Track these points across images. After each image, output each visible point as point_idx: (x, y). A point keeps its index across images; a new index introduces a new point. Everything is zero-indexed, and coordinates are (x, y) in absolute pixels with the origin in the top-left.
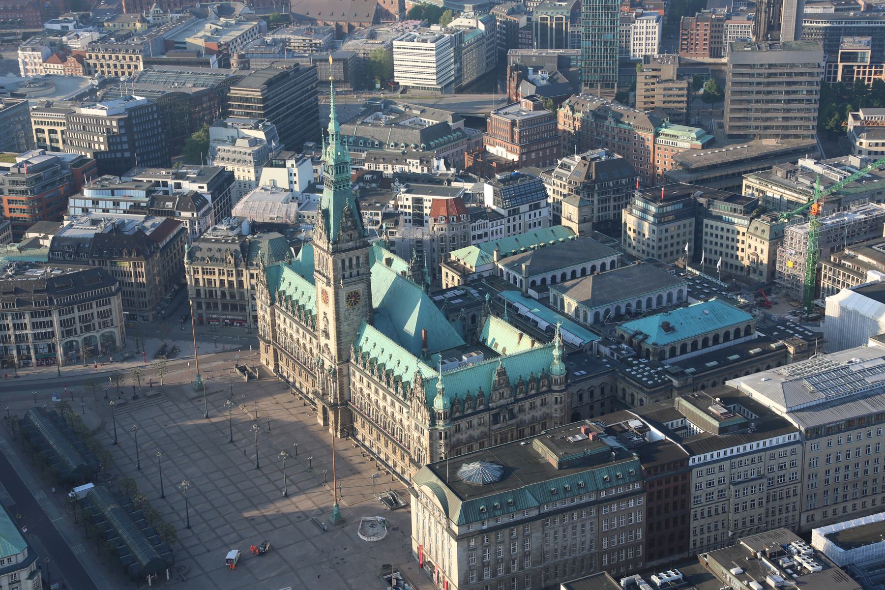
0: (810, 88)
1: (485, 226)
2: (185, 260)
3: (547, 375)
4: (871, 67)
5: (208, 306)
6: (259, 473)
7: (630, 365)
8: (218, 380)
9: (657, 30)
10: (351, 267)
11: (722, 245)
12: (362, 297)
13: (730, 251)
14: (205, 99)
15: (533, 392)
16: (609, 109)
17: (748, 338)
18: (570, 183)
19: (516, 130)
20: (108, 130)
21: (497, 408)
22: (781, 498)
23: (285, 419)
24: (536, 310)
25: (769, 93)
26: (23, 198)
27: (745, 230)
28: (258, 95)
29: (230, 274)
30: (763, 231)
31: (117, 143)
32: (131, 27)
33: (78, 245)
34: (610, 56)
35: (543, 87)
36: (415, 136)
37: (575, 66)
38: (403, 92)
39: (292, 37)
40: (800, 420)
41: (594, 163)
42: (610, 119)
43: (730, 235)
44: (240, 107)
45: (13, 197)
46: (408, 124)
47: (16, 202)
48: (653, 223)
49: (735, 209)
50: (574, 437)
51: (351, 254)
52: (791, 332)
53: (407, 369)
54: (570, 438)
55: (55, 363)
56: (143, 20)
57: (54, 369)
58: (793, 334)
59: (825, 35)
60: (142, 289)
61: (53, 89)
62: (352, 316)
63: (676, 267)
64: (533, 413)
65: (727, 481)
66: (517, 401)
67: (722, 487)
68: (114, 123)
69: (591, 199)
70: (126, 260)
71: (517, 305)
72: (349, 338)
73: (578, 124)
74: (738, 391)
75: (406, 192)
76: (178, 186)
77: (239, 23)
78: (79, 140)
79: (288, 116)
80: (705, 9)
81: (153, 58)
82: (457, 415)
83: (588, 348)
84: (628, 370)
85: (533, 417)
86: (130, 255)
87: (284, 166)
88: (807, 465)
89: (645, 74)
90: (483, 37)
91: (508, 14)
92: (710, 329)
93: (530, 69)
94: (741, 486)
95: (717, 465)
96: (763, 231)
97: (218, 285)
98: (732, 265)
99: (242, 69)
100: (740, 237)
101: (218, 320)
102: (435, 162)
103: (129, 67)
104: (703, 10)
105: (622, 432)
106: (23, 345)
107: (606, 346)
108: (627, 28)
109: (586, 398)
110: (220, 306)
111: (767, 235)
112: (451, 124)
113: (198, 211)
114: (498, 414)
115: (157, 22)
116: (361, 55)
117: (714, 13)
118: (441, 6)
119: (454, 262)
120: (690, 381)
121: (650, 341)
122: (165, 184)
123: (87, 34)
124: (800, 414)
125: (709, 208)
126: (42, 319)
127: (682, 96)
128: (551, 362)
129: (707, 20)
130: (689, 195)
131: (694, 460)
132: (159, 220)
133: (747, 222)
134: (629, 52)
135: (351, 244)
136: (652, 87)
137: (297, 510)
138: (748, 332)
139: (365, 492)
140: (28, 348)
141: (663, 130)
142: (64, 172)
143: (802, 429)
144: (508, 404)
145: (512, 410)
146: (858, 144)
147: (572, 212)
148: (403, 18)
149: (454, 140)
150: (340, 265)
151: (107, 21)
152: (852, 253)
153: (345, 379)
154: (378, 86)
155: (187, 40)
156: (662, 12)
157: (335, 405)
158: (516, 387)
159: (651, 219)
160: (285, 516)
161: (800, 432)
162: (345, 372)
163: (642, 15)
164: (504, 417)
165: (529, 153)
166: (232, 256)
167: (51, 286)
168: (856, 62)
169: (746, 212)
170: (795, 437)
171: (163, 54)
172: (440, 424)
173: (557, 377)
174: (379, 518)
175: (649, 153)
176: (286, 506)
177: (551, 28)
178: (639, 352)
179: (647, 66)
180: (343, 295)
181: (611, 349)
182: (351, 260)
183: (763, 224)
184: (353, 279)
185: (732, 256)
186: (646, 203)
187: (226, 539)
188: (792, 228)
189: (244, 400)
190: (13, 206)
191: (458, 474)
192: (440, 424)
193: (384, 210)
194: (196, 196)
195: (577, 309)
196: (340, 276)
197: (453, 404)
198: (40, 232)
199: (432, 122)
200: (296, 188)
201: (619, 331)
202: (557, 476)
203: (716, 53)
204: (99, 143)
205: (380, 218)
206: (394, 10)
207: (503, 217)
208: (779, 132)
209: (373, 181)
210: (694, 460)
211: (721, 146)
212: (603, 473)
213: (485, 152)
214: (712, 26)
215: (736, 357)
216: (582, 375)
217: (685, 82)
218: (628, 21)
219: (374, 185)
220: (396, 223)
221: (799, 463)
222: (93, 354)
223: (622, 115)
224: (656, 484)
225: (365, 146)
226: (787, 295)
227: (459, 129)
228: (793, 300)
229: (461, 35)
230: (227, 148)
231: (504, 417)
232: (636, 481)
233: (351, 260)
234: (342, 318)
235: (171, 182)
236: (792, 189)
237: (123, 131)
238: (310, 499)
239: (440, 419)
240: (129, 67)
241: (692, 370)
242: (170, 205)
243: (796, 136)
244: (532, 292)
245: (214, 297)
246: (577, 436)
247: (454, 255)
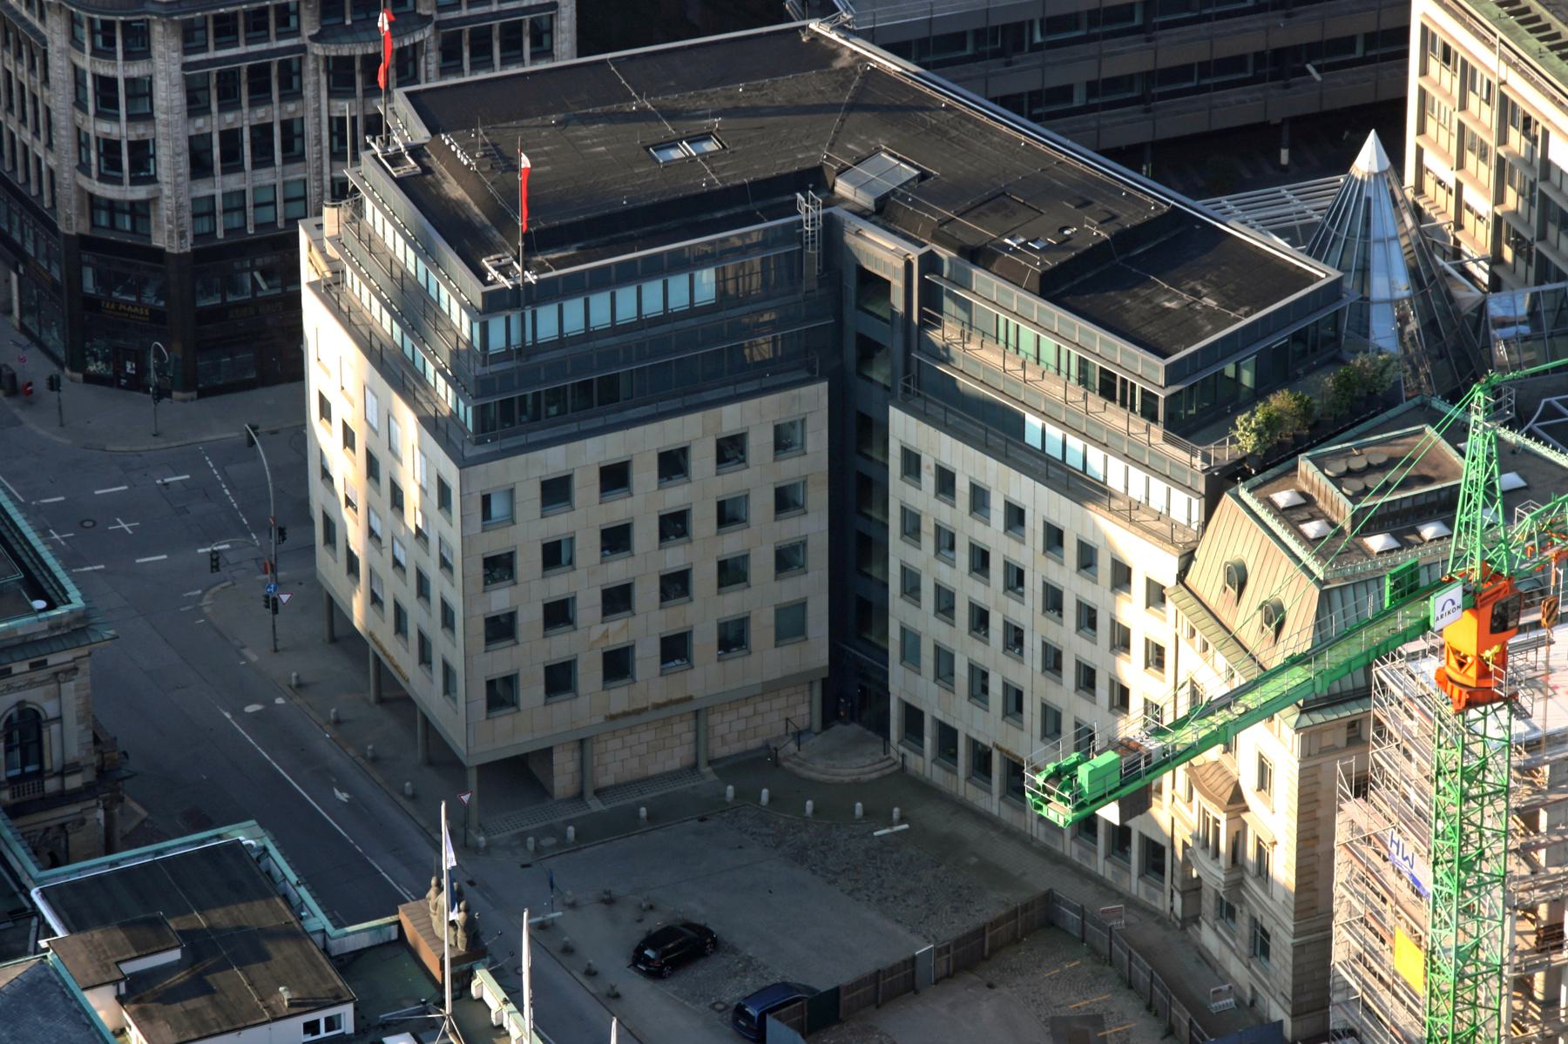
57: (122, 18)
100: (1131, 610)
125: (932, 320)
133: (1184, 507)
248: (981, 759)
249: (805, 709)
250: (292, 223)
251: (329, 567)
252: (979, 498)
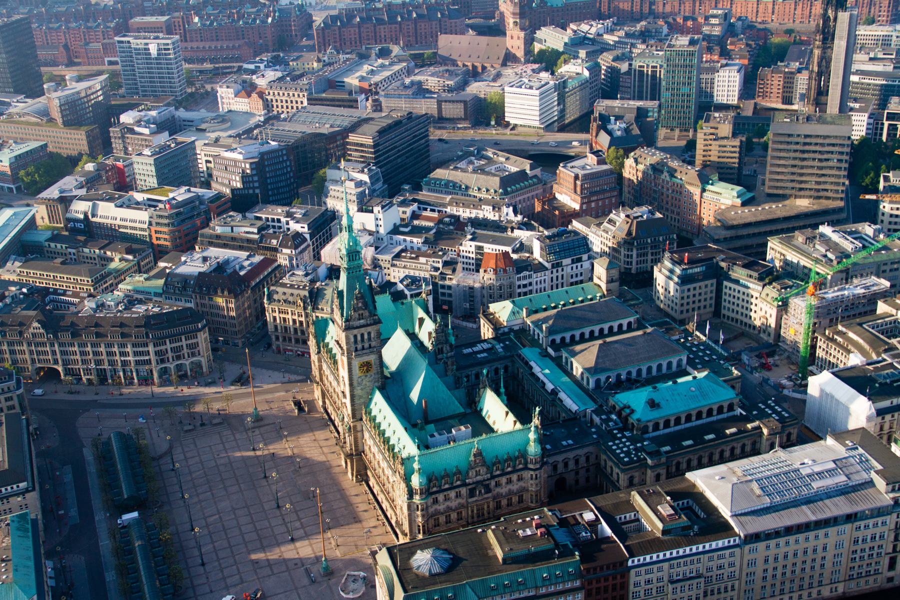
0: (840, 157)
1: (530, 277)
2: (265, 301)
3: (523, 454)
5: (284, 339)
6: (277, 512)
7: (614, 438)
8: (274, 412)
9: (737, 79)
11: (738, 305)
12: (374, 367)
13: (745, 312)
14: (338, 138)
15: (509, 469)
16: (666, 164)
17: (731, 414)
19: (579, 183)
20: (243, 171)
21: (473, 483)
22: (719, 593)
23: (315, 458)
24: (547, 371)
25: (804, 159)
26: (166, 229)
28: (369, 141)
29: (300, 315)
31: (249, 182)
32: (310, 66)
33: (186, 281)
35: (618, 138)
36: (494, 182)
37: (653, 117)
38: (513, 129)
39: (429, 78)
40: (742, 525)
42: (666, 174)
43: (746, 298)
44: (356, 150)
45: (159, 228)
46: (493, 171)
47: (160, 232)
48: (677, 284)
50: (524, 531)
51: (363, 330)
52: (770, 412)
54: (520, 532)
55: (153, 384)
56: (319, 60)
58: (770, 415)
59: (880, 90)
60: (233, 321)
61: (229, 124)
62: (364, 382)
63: (686, 330)
64: (510, 487)
65: (666, 579)
66: (493, 477)
67: (661, 584)
68: (248, 166)
69: (630, 253)
70: (220, 297)
71: (532, 364)
72: (362, 400)
73: (640, 175)
74: (694, 486)
75: (471, 240)
76: (288, 223)
77: (391, 64)
78: (222, 178)
79: (399, 157)
80: (782, 62)
81: (315, 95)
82: (435, 489)
83: (582, 415)
84: (610, 444)
85: (510, 490)
86: (223, 293)
87: (372, 212)
88: (745, 565)
91: (613, 61)
92: (693, 406)
93: (612, 118)
94: (679, 585)
95: (655, 567)
97: (291, 323)
98: (746, 324)
99: (374, 111)
101: (291, 351)
102: (505, 209)
103: (297, 102)
104: (779, 64)
105: (574, 525)
106: (128, 368)
107: (597, 415)
108: (712, 77)
109: (572, 465)
112: (528, 172)
113: (296, 248)
114: (475, 489)
115: (331, 61)
116: (483, 96)
117: (786, 66)
118: (561, 50)
119: (492, 314)
120: (663, 460)
121: (635, 416)
122: (279, 221)
123: (272, 73)
124: (743, 518)
126: (141, 349)
127: (735, 152)
128: (527, 442)
129: (781, 72)
130: (712, 259)
131: (633, 562)
132: (257, 259)
133: (760, 288)
134: (713, 96)
135: (362, 322)
136: (710, 142)
137: (297, 556)
138: (731, 408)
139: (359, 543)
140: (132, 372)
142: (202, 207)
143: (742, 535)
144: (484, 480)
145: (488, 485)
146: (881, 207)
148: (527, 61)
149: (530, 186)
150: (352, 340)
151: (292, 61)
152: (844, 330)
153: (359, 434)
154: (493, 123)
155: (346, 80)
156: (746, 62)
157: (352, 455)
158: (494, 464)
159: (676, 279)
160: (285, 561)
162: (359, 428)
163: (727, 65)
164: (480, 492)
165: (589, 202)
167: (150, 323)
169: (761, 279)
170: (735, 541)
171: (324, 91)
172: (417, 499)
174: (362, 574)
175: (696, 205)
176: (289, 552)
177: (647, 75)
178: (625, 424)
179: (707, 124)
180: (356, 363)
181: (601, 419)
182: (362, 335)
183: (772, 291)
184: (364, 351)
185: (746, 315)
186: (673, 264)
187: (229, 581)
188: (796, 300)
189: (286, 436)
190: (159, 235)
191: (411, 561)
192: (417, 499)
193: (445, 258)
194: (298, 235)
195: (582, 373)
196: (353, 349)
197: (430, 480)
198: (168, 262)
199: (514, 169)
200: (382, 231)
201: (612, 401)
202: (500, 571)
203: (788, 100)
204: (236, 180)
205: (440, 265)
206: (520, 54)
207: (547, 269)
208: (812, 193)
209: (451, 224)
210: (633, 562)
211: (759, 205)
212: (543, 570)
213: (555, 198)
214: (785, 78)
215: (711, 436)
216: (569, 445)
217: (738, 140)
218: (714, 70)
219: (451, 227)
220: (454, 271)
221: (737, 564)
222: (183, 378)
223: (676, 171)
224: (594, 582)
225: (454, 189)
226: (788, 358)
227: (535, 176)
228: (793, 364)
229: (565, 82)
230: (337, 188)
231: (480, 492)
232: (576, 579)
233: (362, 335)
234: (355, 383)
235: (283, 220)
236: (807, 255)
237: (254, 172)
238: (311, 545)
239: (416, 494)
240: (297, 102)
241: (668, 448)
242: (274, 242)
243: (828, 198)
244: (550, 350)
246: (528, 530)
247: (494, 307)
248: (733, 319)
249: (711, 315)
250: (652, 268)
251: (658, 302)
252: (734, 290)
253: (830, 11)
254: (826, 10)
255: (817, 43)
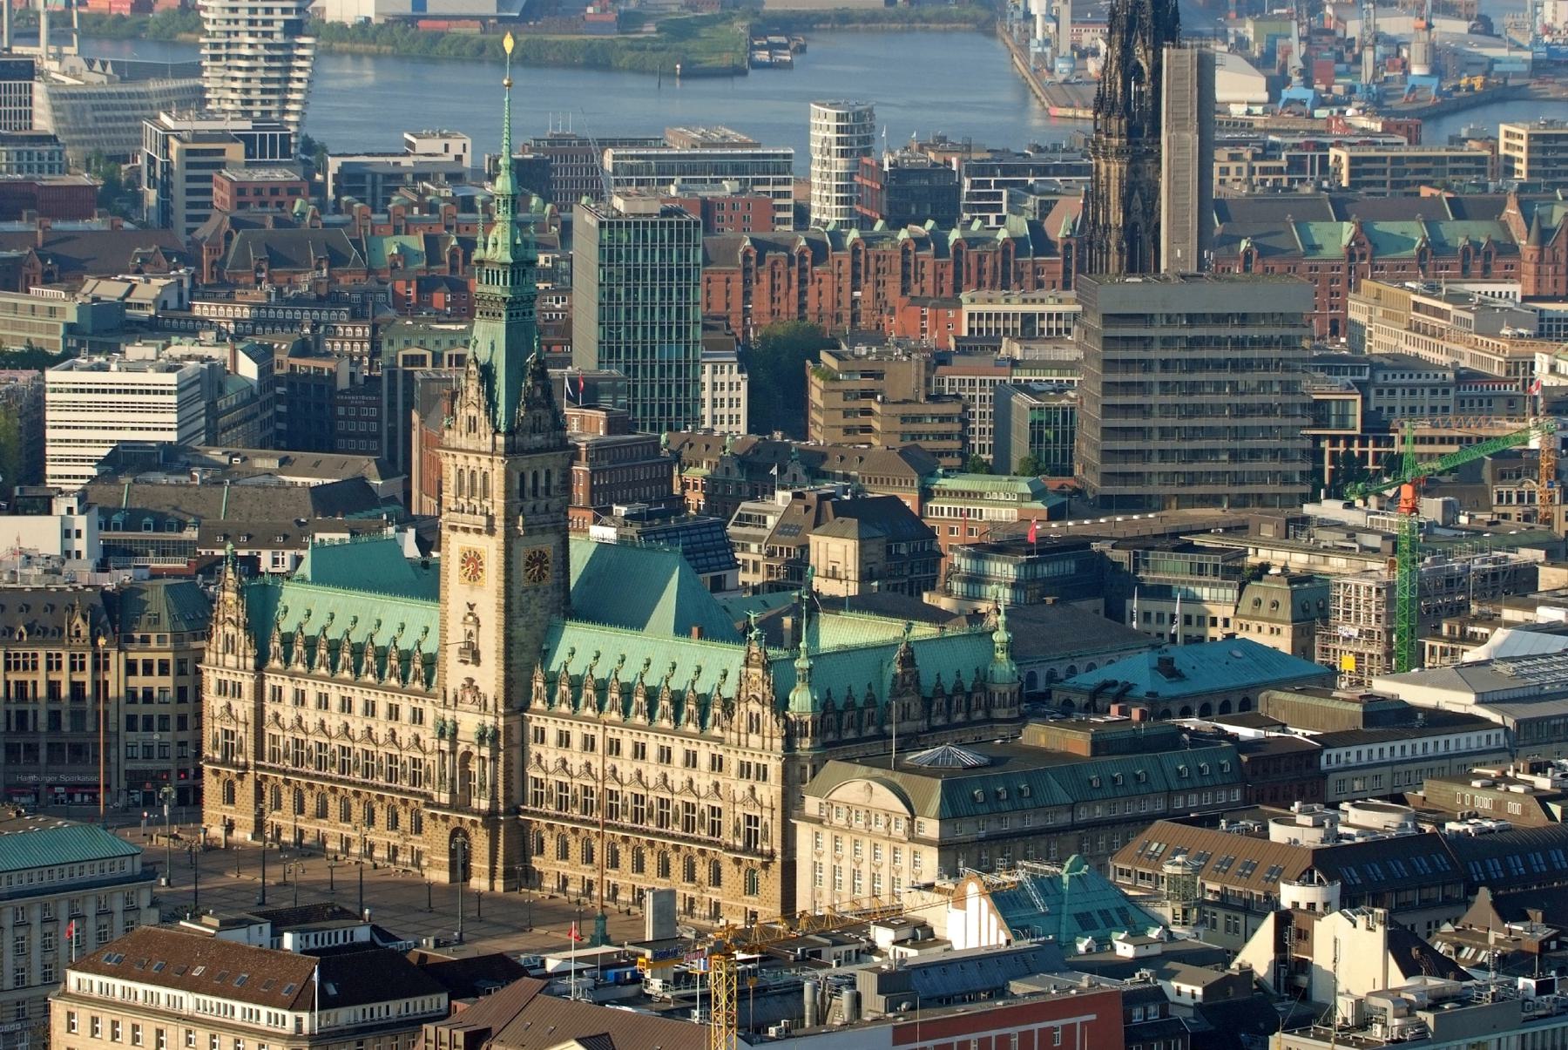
3: (983, 680)
4: (1364, 443)
9: (743, 394)
10: (535, 493)
18: (771, 554)
27: (1229, 612)
30: (1275, 604)
34: (678, 407)
41: (828, 504)
49: (1200, 566)
53: (699, 672)
89: (843, 386)
90: (253, 397)
96: (1275, 604)
110: (43, 752)
111: (1285, 611)
112: (377, 482)
125: (1136, 571)
133: (1231, 594)
141: (942, 481)
147: (840, 558)
161: (1507, 729)
166: (84, 618)
168: (1328, 427)
173: (1003, 689)
180: (522, 552)
234: (516, 607)
239: (804, 734)
245: (30, 728)
253: (1139, 50)
254: (1127, 49)
255: (1115, 141)
